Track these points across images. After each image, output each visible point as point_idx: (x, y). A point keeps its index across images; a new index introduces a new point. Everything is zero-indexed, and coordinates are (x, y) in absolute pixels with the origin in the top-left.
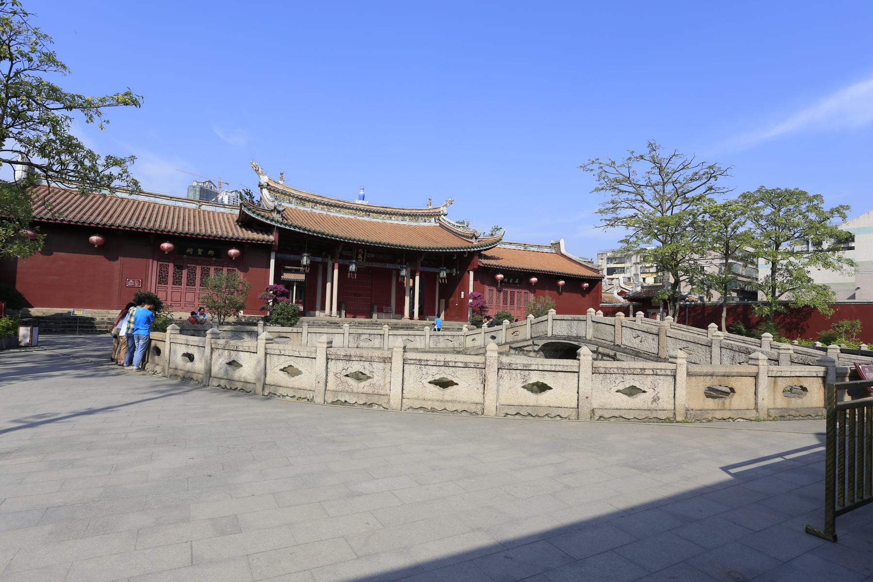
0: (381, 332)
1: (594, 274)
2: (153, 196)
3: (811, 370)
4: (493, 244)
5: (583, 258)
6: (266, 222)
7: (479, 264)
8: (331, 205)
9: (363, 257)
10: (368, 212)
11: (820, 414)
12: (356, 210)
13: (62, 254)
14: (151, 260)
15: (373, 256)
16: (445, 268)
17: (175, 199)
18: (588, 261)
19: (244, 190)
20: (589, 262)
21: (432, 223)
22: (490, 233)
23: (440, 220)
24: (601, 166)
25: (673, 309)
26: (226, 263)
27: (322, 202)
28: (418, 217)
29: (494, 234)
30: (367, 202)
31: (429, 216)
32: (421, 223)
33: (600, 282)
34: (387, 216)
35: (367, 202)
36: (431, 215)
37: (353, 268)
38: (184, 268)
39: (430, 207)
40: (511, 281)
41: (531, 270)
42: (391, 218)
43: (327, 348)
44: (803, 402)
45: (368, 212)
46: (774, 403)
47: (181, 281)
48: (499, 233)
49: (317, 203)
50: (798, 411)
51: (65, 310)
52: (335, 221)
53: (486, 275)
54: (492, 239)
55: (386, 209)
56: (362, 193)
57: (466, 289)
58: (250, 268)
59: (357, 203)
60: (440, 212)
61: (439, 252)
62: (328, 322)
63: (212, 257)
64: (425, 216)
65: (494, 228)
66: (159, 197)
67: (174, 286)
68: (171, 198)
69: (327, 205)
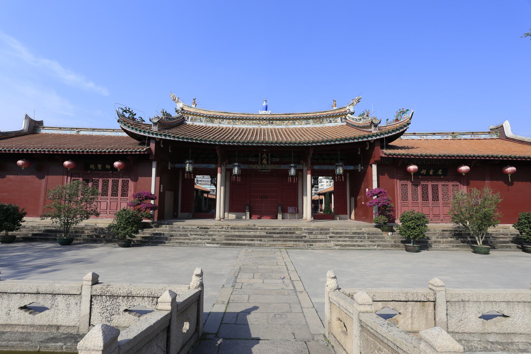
2: (102, 130)
4: (401, 128)
6: (140, 134)
7: (381, 155)
8: (236, 119)
10: (271, 120)
12: (259, 119)
13: (11, 176)
14: (66, 177)
16: (341, 164)
17: (116, 131)
19: (122, 109)
21: (339, 122)
22: (395, 118)
23: (346, 119)
26: (121, 175)
27: (228, 117)
28: (323, 119)
29: (399, 119)
30: (270, 111)
31: (335, 116)
32: (326, 124)
34: (291, 121)
35: (270, 111)
37: (236, 171)
38: (90, 181)
39: (335, 108)
40: (431, 173)
41: (458, 156)
43: (92, 285)
45: (271, 120)
48: (408, 115)
55: (289, 116)
56: (264, 104)
57: (370, 185)
58: (140, 178)
59: (260, 113)
60: (346, 111)
61: (331, 145)
62: (198, 227)
63: (109, 171)
64: (330, 117)
65: (399, 112)
66: (106, 131)
67: (103, 197)
68: (114, 130)
69: (232, 119)
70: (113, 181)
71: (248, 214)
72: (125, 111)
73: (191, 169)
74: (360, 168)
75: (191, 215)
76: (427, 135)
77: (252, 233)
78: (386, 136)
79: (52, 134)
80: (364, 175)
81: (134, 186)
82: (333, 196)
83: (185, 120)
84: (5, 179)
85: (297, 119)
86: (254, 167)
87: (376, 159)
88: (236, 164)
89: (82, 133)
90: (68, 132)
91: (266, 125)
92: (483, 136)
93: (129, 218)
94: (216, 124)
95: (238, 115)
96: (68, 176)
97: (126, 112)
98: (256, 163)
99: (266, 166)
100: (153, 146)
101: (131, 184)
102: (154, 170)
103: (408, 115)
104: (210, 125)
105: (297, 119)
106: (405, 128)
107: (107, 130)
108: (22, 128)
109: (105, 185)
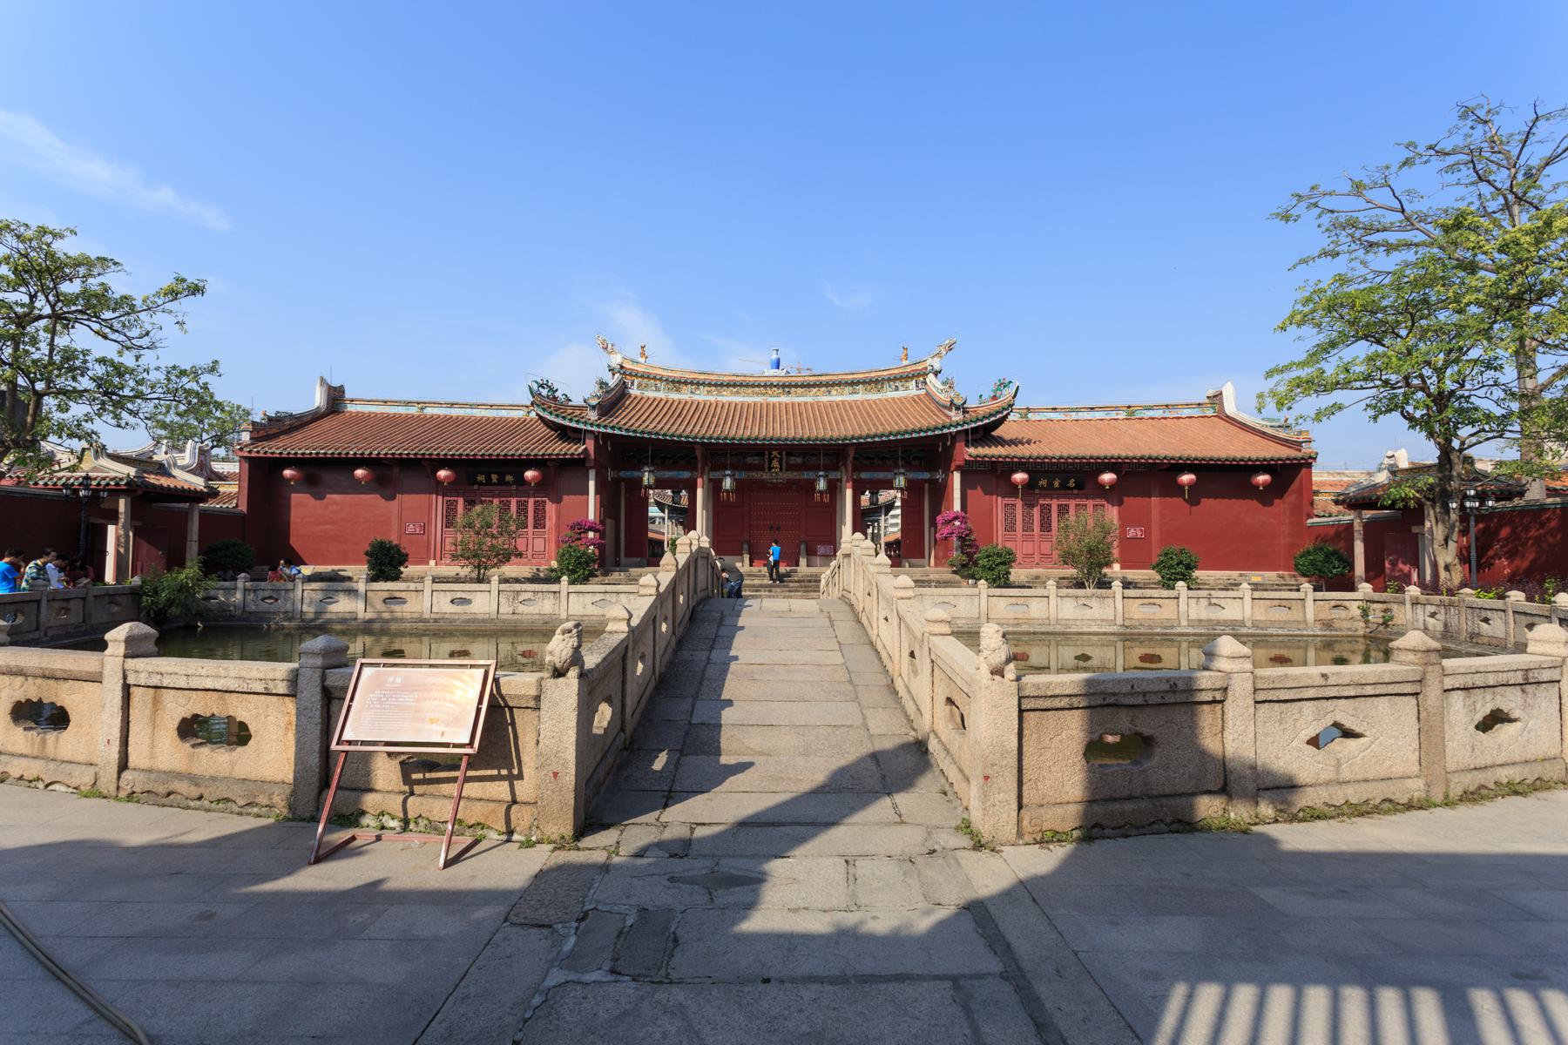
0: (1044, 592)
1: (1292, 453)
3: (244, 674)
5: (1269, 420)
8: (722, 385)
9: (781, 464)
10: (786, 387)
11: (262, 800)
12: (765, 386)
13: (335, 496)
15: (799, 460)
16: (902, 470)
18: (1278, 424)
19: (536, 382)
20: (1279, 427)
22: (992, 394)
24: (1312, 201)
25: (1444, 522)
31: (905, 378)
32: (889, 394)
33: (1304, 470)
34: (823, 389)
36: (908, 377)
37: (728, 483)
39: (905, 363)
40: (1056, 484)
42: (830, 392)
44: (233, 764)
45: (786, 387)
46: (152, 756)
47: (1050, 526)
48: (1008, 393)
49: (698, 384)
50: (197, 785)
51: (336, 567)
52: (735, 410)
53: (991, 476)
54: (995, 406)
55: (819, 378)
56: (774, 356)
58: (565, 497)
59: (767, 374)
64: (895, 379)
69: (716, 385)
70: (517, 502)
71: (747, 557)
72: (541, 386)
73: (652, 482)
74: (939, 476)
75: (645, 561)
76: (1077, 410)
77: (757, 582)
78: (973, 425)
79: (370, 414)
80: (940, 493)
81: (556, 510)
82: (623, 487)
83: (626, 387)
84: (325, 501)
85: (834, 384)
86: (757, 475)
87: (958, 463)
88: (728, 472)
89: (429, 411)
90: (402, 410)
91: (778, 395)
92: (1186, 412)
93: (580, 557)
94: (685, 395)
95: (725, 379)
96: (437, 495)
97: (543, 388)
98: (760, 468)
99: (777, 474)
100: (590, 444)
101: (551, 508)
102: (592, 484)
103: (1008, 393)
104: (674, 396)
105: (834, 384)
106: (1005, 413)
107: (478, 406)
108: (317, 405)
109: (522, 509)
